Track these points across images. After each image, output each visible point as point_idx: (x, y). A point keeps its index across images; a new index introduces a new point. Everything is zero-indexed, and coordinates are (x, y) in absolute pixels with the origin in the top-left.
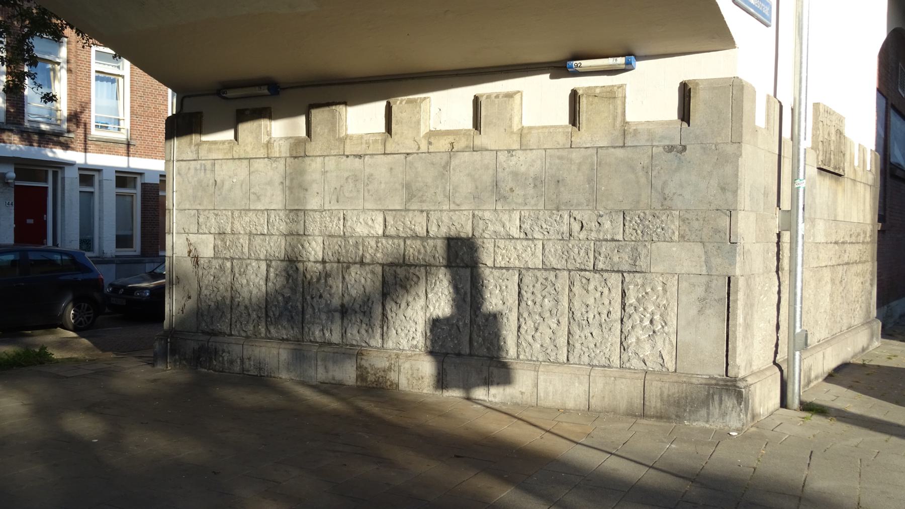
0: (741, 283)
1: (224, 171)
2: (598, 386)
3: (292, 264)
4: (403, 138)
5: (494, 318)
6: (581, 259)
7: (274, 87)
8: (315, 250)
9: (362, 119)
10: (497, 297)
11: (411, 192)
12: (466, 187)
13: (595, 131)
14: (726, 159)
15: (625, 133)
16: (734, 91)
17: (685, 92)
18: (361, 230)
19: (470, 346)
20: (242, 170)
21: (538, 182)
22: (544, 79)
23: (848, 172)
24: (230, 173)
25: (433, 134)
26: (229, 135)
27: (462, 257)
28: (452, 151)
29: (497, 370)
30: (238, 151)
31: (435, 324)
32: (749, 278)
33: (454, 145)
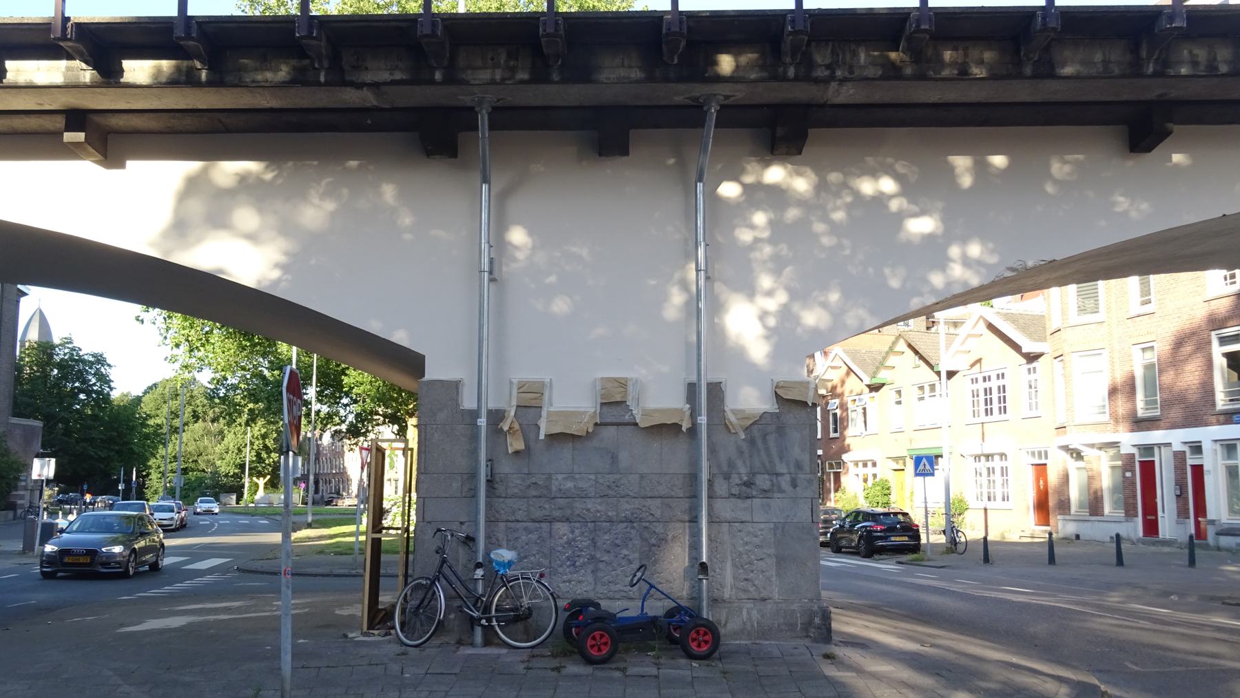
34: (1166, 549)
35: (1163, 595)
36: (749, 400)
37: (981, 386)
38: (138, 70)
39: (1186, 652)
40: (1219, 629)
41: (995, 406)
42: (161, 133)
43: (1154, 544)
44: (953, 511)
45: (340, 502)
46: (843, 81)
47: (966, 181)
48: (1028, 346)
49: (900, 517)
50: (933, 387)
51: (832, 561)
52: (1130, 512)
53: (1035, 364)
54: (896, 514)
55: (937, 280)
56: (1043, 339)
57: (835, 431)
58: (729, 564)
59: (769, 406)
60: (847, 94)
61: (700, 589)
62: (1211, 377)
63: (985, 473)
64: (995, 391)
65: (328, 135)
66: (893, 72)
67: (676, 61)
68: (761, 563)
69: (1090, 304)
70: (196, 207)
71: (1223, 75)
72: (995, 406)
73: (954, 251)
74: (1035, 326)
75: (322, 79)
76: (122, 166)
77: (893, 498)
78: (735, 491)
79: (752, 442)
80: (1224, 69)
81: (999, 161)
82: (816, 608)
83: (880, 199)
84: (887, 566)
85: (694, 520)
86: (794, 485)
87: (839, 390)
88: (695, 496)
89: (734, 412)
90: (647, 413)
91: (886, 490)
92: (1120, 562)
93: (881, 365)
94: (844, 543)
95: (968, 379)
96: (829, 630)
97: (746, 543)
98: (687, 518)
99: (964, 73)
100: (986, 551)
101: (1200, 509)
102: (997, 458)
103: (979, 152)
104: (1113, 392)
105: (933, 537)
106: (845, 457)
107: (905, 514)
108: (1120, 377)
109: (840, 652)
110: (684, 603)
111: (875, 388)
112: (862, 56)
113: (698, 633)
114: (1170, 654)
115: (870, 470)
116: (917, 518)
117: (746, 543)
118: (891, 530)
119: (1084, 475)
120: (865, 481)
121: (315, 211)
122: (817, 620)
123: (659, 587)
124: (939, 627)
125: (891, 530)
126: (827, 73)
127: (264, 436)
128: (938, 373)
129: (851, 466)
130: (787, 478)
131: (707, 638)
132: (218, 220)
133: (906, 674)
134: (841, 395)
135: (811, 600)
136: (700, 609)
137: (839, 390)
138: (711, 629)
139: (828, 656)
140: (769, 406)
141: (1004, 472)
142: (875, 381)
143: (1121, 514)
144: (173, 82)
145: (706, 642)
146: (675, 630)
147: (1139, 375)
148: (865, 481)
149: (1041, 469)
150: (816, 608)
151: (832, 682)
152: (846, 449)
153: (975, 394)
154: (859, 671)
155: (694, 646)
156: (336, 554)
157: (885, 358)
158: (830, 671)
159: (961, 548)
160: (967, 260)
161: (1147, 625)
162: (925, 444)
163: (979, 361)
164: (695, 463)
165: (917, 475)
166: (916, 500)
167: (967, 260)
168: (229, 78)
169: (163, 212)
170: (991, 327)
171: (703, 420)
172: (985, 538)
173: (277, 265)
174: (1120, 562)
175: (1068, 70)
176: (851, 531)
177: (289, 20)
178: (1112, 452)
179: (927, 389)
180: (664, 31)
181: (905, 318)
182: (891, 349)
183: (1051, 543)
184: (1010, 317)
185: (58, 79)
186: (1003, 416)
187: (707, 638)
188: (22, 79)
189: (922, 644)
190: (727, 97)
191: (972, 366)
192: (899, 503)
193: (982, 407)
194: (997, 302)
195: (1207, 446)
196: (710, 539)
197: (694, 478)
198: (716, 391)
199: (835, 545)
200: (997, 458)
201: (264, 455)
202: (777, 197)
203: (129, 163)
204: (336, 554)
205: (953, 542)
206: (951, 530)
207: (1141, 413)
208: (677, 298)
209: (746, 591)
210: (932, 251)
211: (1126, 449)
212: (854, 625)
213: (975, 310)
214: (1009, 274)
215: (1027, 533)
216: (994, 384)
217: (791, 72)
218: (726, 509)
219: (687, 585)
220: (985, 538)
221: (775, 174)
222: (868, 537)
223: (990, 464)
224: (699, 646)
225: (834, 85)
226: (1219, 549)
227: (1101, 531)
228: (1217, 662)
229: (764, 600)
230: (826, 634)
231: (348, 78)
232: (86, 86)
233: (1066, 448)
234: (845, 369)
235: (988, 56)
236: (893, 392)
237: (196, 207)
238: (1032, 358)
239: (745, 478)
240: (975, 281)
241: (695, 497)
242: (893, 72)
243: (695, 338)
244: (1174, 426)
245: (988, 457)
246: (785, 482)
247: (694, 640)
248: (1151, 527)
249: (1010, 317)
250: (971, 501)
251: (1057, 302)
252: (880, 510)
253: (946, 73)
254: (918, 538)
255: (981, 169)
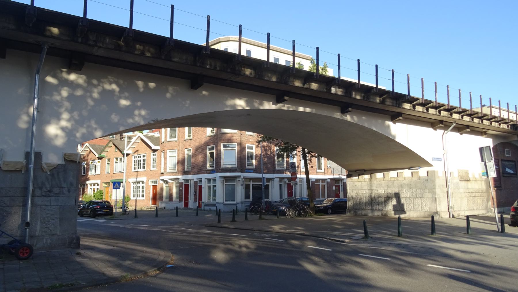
0: (437, 199)
1: (357, 183)
2: (418, 214)
3: (371, 197)
4: (387, 178)
5: (403, 204)
6: (414, 195)
7: (365, 170)
8: (373, 195)
9: (380, 175)
10: (403, 201)
11: (388, 186)
12: (397, 186)
13: (415, 178)
14: (434, 182)
15: (419, 178)
16: (434, 172)
17: (428, 172)
18: (380, 192)
19: (400, 208)
20: (360, 183)
21: (407, 185)
22: (407, 170)
23: (471, 179)
24: (358, 184)
25: (391, 178)
26: (357, 177)
27: (397, 196)
28: (394, 180)
29: (403, 212)
30: (359, 180)
31: (394, 206)
32: (439, 198)
33: (394, 180)
34: (190, 211)
35: (189, 225)
36: (53, 159)
37: (137, 159)
39: (196, 241)
40: (205, 234)
41: (142, 166)
43: (187, 209)
44: (125, 200)
46: (99, 47)
47: (142, 90)
48: (154, 147)
49: (106, 203)
50: (121, 159)
51: (80, 220)
52: (181, 200)
53: (156, 153)
54: (105, 202)
55: (130, 121)
56: (158, 145)
57: (84, 173)
58: (39, 223)
59: (61, 162)
60: (101, 52)
61: (26, 232)
62: (206, 160)
63: (136, 188)
64: (137, 161)
66: (118, 48)
67: (31, 25)
68: (53, 221)
69: (173, 135)
71: (218, 70)
72: (142, 166)
73: (136, 112)
74: (156, 141)
77: (104, 197)
78: (44, 194)
79: (52, 175)
80: (218, 68)
81: (152, 85)
82: (74, 237)
83: (113, 91)
84: (101, 220)
85: (25, 205)
86: (69, 191)
87: (86, 158)
88: (26, 196)
89: (46, 164)
90: (7, 164)
91: (101, 193)
92: (177, 215)
93: (103, 150)
94: (85, 213)
95: (133, 157)
96: (79, 244)
97: (47, 214)
98: (21, 205)
99: (143, 54)
100: (136, 214)
101: (200, 199)
102: (141, 183)
103: (146, 81)
104: (178, 162)
105: (117, 210)
106: (87, 182)
107: (108, 202)
108: (181, 158)
109: (82, 252)
110: (17, 238)
111: (100, 158)
112: (108, 40)
113: (23, 250)
114: (191, 242)
115: (96, 187)
116: (113, 203)
117: (47, 214)
118: (103, 208)
119: (168, 188)
120: (94, 191)
122: (75, 241)
123: (7, 233)
124: (119, 240)
125: (103, 208)
126: (94, 43)
128: (124, 154)
129: (89, 185)
130: (66, 189)
131: (27, 251)
133: (107, 257)
134: (87, 160)
135: (73, 234)
136: (25, 240)
137: (86, 158)
138: (30, 248)
139: (79, 254)
140: (61, 162)
141: (143, 187)
142: (100, 156)
143: (178, 200)
145: (27, 253)
146: (13, 249)
147: (186, 156)
148: (94, 191)
149: (155, 187)
150: (74, 237)
151: (79, 263)
152: (88, 179)
153: (135, 162)
154: (90, 258)
155: (21, 255)
157: (105, 148)
158: (79, 259)
159: (127, 213)
160: (141, 115)
161: (185, 234)
162: (116, 178)
163: (137, 151)
164: (27, 183)
165: (114, 188)
166: (114, 197)
167: (141, 115)
170: (142, 140)
171: (32, 166)
172: (136, 209)
174: (177, 215)
175: (176, 60)
176: (88, 208)
178: (177, 181)
179: (119, 159)
180: (27, 12)
181: (112, 134)
182: (107, 145)
183: (157, 210)
184: (148, 137)
186: (144, 170)
187: (27, 251)
189: (111, 245)
190: (52, 44)
191: (135, 152)
192: (105, 198)
193: (137, 166)
194: (145, 132)
195: (203, 180)
196: (31, 213)
197: (26, 189)
198: (38, 155)
199: (81, 214)
200: (141, 183)
202: (72, 85)
205: (125, 211)
206: (124, 207)
207: (186, 170)
208: (25, 118)
209: (45, 232)
210: (129, 111)
211: (181, 181)
212: (88, 242)
213: (137, 133)
214: (152, 122)
215: (149, 207)
216: (142, 159)
217: (80, 40)
218: (39, 201)
219: (20, 231)
220: (136, 209)
221: (73, 77)
222: (94, 210)
223: (138, 185)
224: (23, 255)
225: (96, 48)
226: (204, 210)
227: (172, 206)
228: (204, 243)
229: (53, 235)
230: (78, 245)
233: (163, 180)
234: (89, 150)
235: (152, 50)
236: (107, 160)
238: (154, 151)
239: (49, 189)
240: (142, 123)
241: (26, 196)
242: (118, 48)
243: (31, 134)
244: (195, 174)
245: (138, 183)
246: (65, 191)
247: (21, 252)
248: (186, 204)
249: (148, 137)
250: (132, 198)
251: (164, 133)
252: (99, 201)
253: (136, 52)
254: (113, 210)
255: (146, 86)
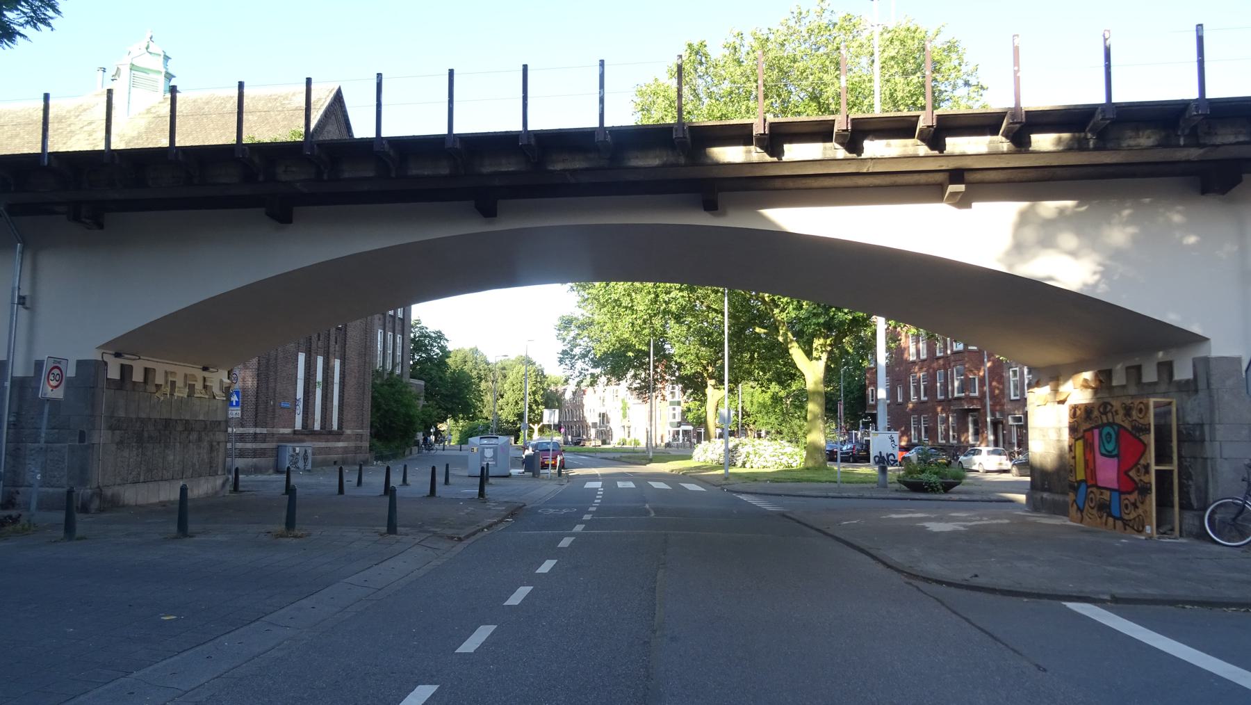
38: (1043, 142)
42: (998, 182)
45: (587, 444)
65: (1136, 180)
70: (1030, 234)
75: (1182, 143)
76: (970, 206)
121: (1119, 234)
127: (534, 393)
132: (1047, 242)
144: (1069, 149)
156: (772, 481)
168: (1109, 145)
169: (1007, 241)
173: (1095, 273)
177: (1183, 105)
185: (984, 150)
188: (957, 151)
201: (534, 407)
203: (974, 205)
204: (772, 481)
231: (1202, 141)
232: (1003, 153)
237: (1030, 234)
